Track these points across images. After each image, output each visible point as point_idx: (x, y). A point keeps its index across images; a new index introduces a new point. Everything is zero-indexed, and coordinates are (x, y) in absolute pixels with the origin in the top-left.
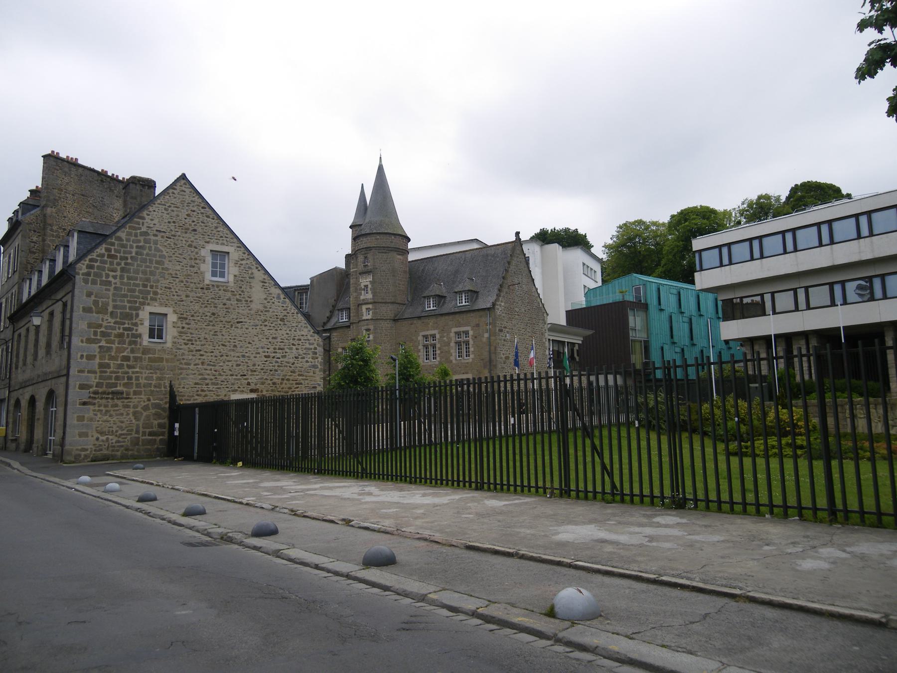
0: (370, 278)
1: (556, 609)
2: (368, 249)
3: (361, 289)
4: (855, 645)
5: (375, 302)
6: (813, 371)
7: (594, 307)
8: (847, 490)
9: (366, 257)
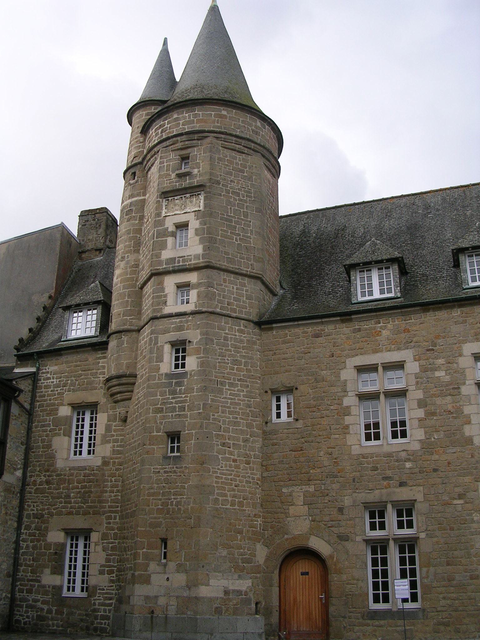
3: (165, 233)
5: (208, 267)
9: (185, 159)
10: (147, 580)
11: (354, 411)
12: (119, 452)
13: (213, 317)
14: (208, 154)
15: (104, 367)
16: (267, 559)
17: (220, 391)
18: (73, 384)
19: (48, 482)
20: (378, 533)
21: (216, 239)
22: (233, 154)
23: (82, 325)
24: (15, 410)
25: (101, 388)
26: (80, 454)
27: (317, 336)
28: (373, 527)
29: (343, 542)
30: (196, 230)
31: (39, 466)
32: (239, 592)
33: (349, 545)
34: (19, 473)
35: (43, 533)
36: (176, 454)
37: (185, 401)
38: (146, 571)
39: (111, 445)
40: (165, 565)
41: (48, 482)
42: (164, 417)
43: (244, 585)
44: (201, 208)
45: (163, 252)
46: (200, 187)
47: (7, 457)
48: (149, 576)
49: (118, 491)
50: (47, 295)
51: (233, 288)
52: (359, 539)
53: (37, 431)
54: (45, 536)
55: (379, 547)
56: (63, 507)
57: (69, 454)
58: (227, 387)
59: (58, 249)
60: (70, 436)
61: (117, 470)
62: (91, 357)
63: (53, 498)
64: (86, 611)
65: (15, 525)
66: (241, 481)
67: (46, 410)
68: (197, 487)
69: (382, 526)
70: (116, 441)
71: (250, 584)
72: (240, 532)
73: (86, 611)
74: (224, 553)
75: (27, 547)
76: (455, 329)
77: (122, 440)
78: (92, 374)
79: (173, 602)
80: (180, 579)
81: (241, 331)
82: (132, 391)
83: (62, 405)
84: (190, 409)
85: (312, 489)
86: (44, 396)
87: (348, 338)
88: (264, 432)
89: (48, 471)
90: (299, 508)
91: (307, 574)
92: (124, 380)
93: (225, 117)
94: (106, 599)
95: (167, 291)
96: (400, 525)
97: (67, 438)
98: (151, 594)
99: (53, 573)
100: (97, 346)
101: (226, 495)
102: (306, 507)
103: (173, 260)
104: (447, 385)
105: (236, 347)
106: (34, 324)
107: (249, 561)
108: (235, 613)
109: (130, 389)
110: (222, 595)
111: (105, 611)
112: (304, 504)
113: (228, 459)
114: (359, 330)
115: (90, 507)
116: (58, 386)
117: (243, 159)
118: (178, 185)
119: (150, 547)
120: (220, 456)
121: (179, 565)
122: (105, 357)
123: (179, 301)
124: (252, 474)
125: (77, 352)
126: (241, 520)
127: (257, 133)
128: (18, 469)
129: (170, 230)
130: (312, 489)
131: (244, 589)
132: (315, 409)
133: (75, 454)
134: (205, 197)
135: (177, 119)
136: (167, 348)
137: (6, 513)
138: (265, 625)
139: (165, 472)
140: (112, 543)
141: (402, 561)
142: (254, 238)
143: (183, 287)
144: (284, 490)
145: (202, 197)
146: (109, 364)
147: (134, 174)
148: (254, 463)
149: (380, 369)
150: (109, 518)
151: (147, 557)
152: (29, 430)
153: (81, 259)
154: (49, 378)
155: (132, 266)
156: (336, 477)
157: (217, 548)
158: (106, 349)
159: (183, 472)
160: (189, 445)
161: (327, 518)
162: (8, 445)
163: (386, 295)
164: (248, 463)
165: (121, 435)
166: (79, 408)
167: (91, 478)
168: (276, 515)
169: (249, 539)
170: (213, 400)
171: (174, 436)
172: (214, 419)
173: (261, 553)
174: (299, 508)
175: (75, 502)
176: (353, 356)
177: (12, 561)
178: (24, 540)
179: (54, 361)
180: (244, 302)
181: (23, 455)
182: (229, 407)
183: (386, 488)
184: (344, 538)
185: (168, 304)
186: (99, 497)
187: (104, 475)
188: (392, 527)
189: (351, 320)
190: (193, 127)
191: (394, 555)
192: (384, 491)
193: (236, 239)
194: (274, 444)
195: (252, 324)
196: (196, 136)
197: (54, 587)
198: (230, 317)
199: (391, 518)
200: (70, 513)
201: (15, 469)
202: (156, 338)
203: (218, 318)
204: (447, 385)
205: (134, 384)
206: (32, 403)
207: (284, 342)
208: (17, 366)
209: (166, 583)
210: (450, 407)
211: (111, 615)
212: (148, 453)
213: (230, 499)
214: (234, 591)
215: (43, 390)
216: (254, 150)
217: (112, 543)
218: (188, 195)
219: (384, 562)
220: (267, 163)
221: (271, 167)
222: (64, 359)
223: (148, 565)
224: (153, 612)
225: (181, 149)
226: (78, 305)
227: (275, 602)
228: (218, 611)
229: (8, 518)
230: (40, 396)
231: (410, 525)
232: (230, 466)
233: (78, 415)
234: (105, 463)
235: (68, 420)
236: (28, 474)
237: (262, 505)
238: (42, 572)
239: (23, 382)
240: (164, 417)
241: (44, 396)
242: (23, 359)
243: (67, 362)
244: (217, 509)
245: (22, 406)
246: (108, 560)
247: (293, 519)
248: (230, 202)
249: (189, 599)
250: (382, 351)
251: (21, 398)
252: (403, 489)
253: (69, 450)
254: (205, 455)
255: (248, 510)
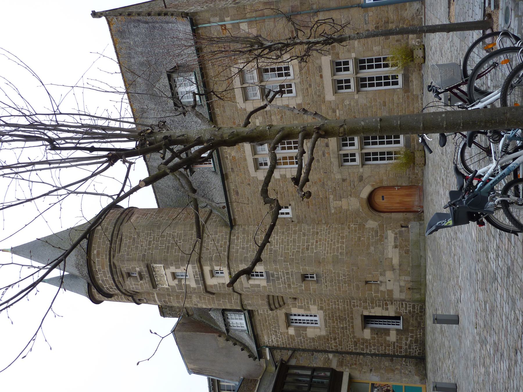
0: (159, 268)
1: (411, 368)
2: (112, 268)
3: (180, 286)
4: (423, 125)
5: (199, 261)
6: (105, 141)
7: (126, 70)
8: (222, 193)
9: (129, 275)
10: (391, 292)
11: (283, 172)
12: (315, 301)
13: (231, 257)
14: (125, 262)
15: (263, 311)
16: (375, 220)
17: (276, 251)
18: (275, 327)
19: (335, 339)
20: (358, 157)
21: (182, 257)
22: (123, 245)
23: (238, 322)
24: (293, 362)
25: (276, 312)
26: (317, 321)
27: (237, 193)
28: (348, 87)
29: (364, 179)
30: (176, 268)
31: (325, 344)
32: (395, 238)
33: (365, 176)
34: (331, 356)
35: (365, 341)
36: (315, 276)
37: (283, 272)
38: (385, 292)
39: (310, 306)
40: (381, 282)
41: (335, 339)
42: (293, 283)
43: (391, 235)
44: (162, 265)
45: (192, 286)
46: (148, 266)
47: (322, 366)
48: (388, 290)
49: (338, 301)
50: (219, 339)
51: (211, 244)
52: (361, 170)
53: (305, 346)
54: (367, 340)
55: (366, 157)
56: (349, 330)
57: (317, 328)
58: (273, 247)
59: (189, 333)
60: (306, 327)
61: (325, 302)
62: (257, 318)
63: (344, 336)
64: (410, 317)
65: (361, 356)
66: (329, 238)
67: (291, 341)
68: (334, 266)
69: (353, 155)
70: (308, 303)
71: (390, 231)
72: (359, 238)
73: (410, 317)
74: (372, 248)
75: (374, 349)
76: (228, 112)
77: (307, 300)
78: (268, 317)
79: (403, 278)
80: (389, 275)
81: (238, 238)
82: (278, 296)
83: (288, 333)
84: (288, 269)
85: (332, 197)
86: (283, 343)
87: (238, 175)
88: (298, 222)
89: (328, 339)
90: (344, 203)
91: (383, 197)
92: (271, 302)
93: (98, 252)
94: (402, 307)
95: (216, 283)
96: (347, 69)
97: (308, 329)
98: (399, 289)
99: (389, 335)
100: (251, 316)
101: (338, 247)
102: (342, 199)
103: (197, 281)
104: (265, 118)
105: (248, 242)
106: (238, 348)
107: (377, 232)
108: (408, 241)
109: (276, 298)
110: (397, 250)
111: (410, 307)
112: (341, 200)
113: (316, 246)
114: (232, 169)
115: (348, 316)
116: (276, 336)
117: (126, 238)
118: (148, 279)
119: (371, 290)
120: (315, 251)
121: (381, 275)
122: (257, 311)
123: (222, 275)
124: (324, 231)
125: (255, 325)
126: (352, 237)
127: (107, 229)
128: (328, 357)
129: (177, 283)
130: (332, 197)
131: (393, 235)
132: (283, 195)
133: (317, 323)
134: (155, 263)
135: (103, 281)
136: (251, 282)
137: (355, 364)
138: (415, 221)
139: (326, 282)
140: (369, 304)
141: (370, 67)
142: (178, 230)
143: (213, 274)
144: (333, 211)
145: (155, 265)
146: (262, 309)
147: (139, 300)
148: (317, 229)
149: (256, 157)
150: (354, 306)
151: (377, 291)
152: (304, 350)
153: (192, 315)
154: (272, 340)
155: (201, 300)
156: (323, 183)
157: (369, 253)
158: (252, 311)
159: (325, 273)
160: (309, 270)
161: (349, 188)
162: (315, 365)
163: (212, 162)
164: (317, 233)
165: (304, 300)
166: (289, 322)
167: (331, 317)
168: (348, 216)
169: (363, 232)
170: (281, 257)
171: (304, 277)
172: (293, 255)
173: (372, 224)
174: (344, 203)
175: (346, 324)
176: (249, 172)
177: (383, 358)
178: (371, 351)
179: (261, 338)
180: (219, 237)
181: (320, 353)
182: (285, 245)
183: (329, 155)
184: (361, 179)
185: (224, 282)
186: (342, 311)
187: (329, 309)
188: (349, 75)
189: (226, 174)
190: (107, 271)
191: (366, 73)
192: (331, 156)
193: (180, 243)
194: (305, 217)
195: (233, 231)
196: (114, 270)
197: (397, 334)
198: (229, 246)
199: (342, 75)
200: (353, 327)
201: (329, 359)
202: (246, 288)
203: (231, 254)
204: (265, 118)
205: (273, 296)
206: (288, 349)
207: (242, 211)
208: (266, 358)
209: (392, 282)
210: (279, 117)
211: (412, 304)
212: (315, 292)
213: (340, 245)
214: (395, 242)
215: (279, 343)
216: (118, 231)
217: (369, 304)
218: (154, 273)
219: (375, 154)
220: (126, 220)
221: (128, 217)
222: (259, 333)
223: (382, 291)
224: (409, 288)
225: (123, 277)
226: (226, 325)
227: (400, 216)
228: (407, 252)
229: (358, 363)
230: (283, 344)
231: (346, 63)
232: (320, 245)
233: (293, 322)
234: (321, 308)
235: (297, 329)
236: (331, 350)
237: (342, 224)
238: (389, 341)
239: (276, 357)
240: (293, 283)
241: (283, 343)
242: (261, 355)
243: (262, 331)
244: (347, 253)
245: (291, 357)
246: (379, 306)
247: (350, 207)
248: (156, 247)
249: (400, 270)
250: (245, 156)
251: (285, 358)
252: (330, 145)
253: (314, 328)
254: (315, 261)
255: (346, 233)
